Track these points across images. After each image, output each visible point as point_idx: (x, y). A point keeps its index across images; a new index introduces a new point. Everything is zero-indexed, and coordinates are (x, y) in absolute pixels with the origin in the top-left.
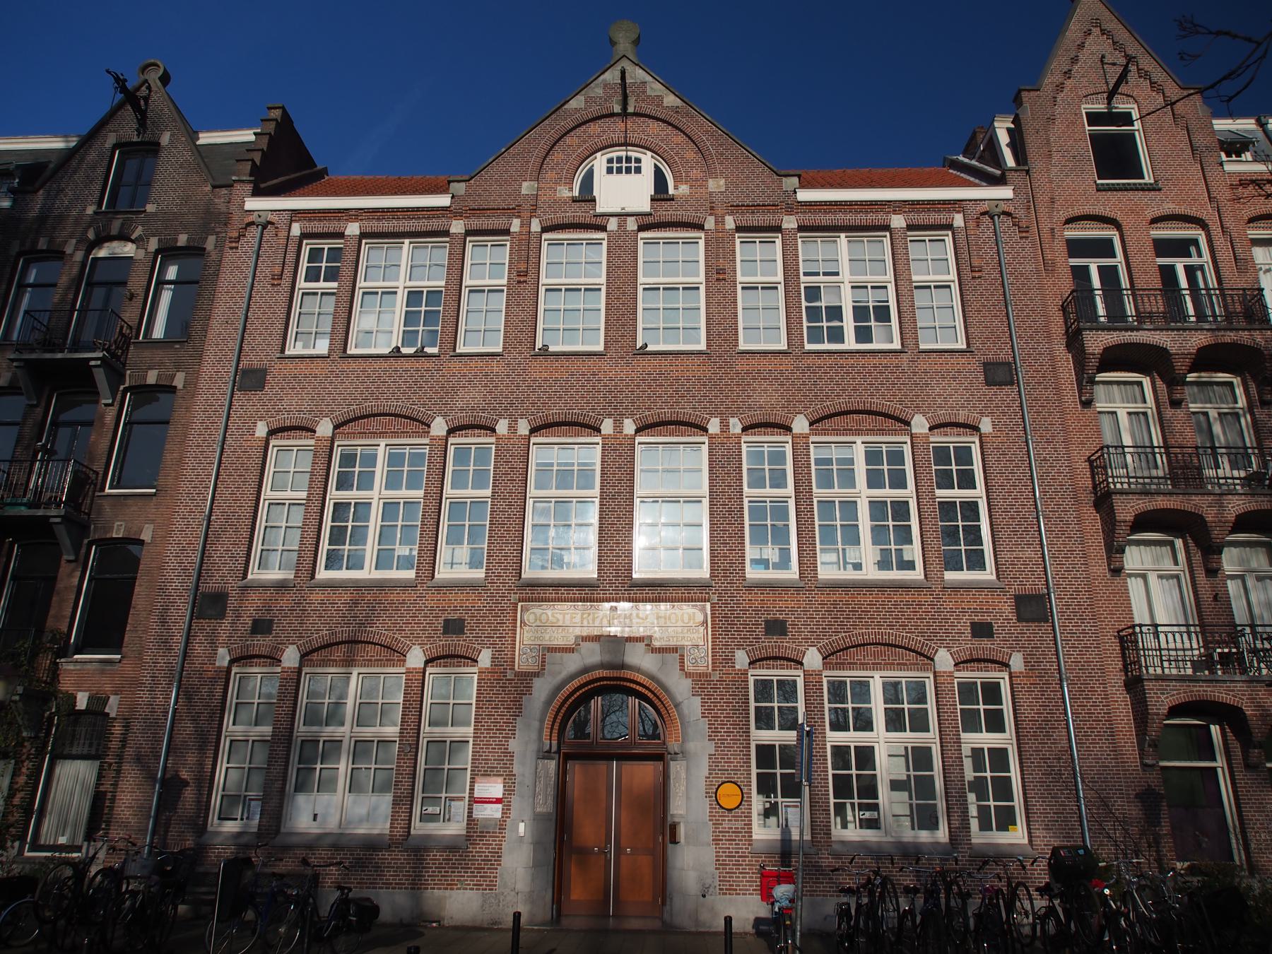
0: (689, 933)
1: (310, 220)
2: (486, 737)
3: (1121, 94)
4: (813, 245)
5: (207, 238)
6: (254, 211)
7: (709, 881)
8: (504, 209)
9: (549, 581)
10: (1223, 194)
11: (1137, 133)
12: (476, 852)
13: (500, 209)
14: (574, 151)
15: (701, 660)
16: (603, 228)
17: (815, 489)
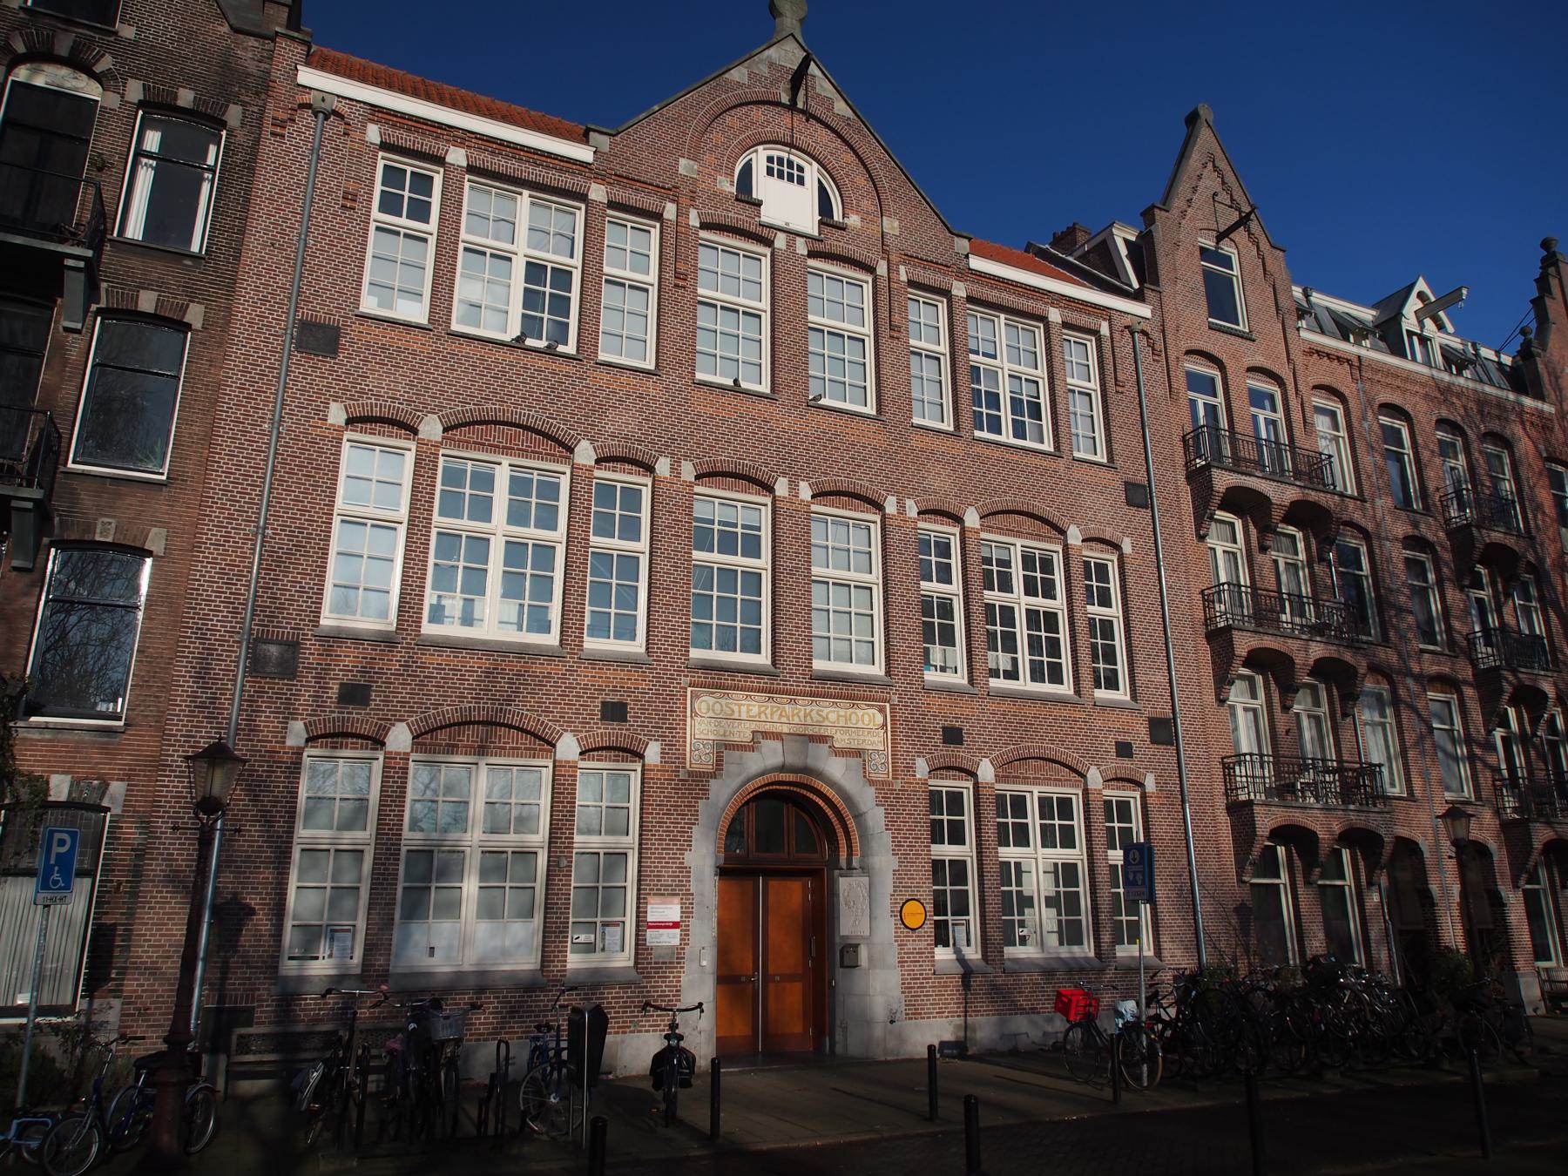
0: (881, 1062)
1: (394, 126)
2: (658, 849)
3: (1231, 240)
4: (484, 197)
5: (227, 106)
6: (311, 88)
7: (895, 1007)
8: (658, 186)
9: (716, 664)
10: (1299, 359)
11: (1235, 279)
12: (651, 987)
13: (652, 185)
14: (736, 136)
15: (881, 769)
16: (768, 243)
17: (436, 517)
